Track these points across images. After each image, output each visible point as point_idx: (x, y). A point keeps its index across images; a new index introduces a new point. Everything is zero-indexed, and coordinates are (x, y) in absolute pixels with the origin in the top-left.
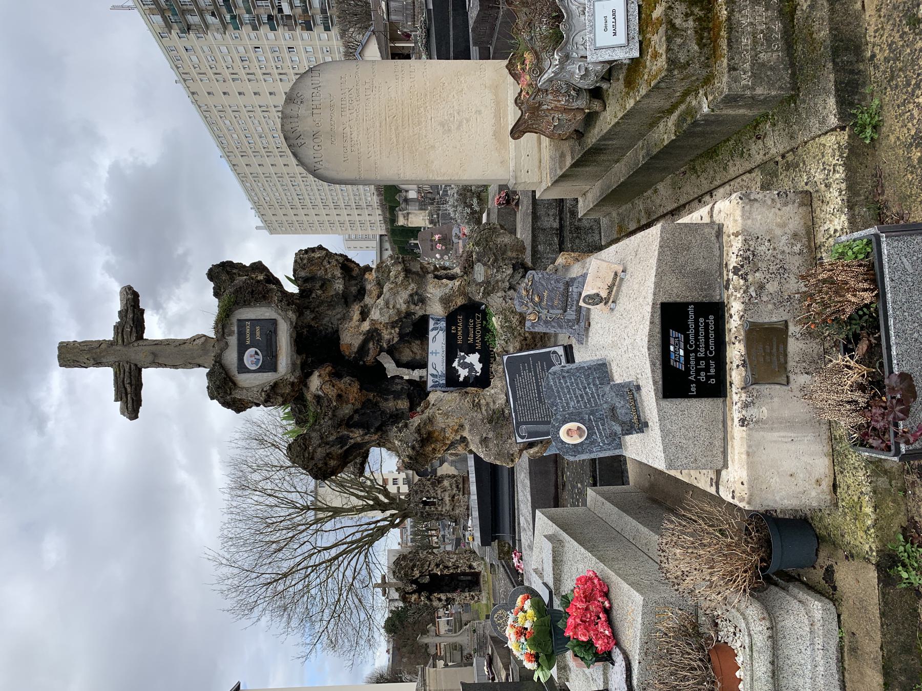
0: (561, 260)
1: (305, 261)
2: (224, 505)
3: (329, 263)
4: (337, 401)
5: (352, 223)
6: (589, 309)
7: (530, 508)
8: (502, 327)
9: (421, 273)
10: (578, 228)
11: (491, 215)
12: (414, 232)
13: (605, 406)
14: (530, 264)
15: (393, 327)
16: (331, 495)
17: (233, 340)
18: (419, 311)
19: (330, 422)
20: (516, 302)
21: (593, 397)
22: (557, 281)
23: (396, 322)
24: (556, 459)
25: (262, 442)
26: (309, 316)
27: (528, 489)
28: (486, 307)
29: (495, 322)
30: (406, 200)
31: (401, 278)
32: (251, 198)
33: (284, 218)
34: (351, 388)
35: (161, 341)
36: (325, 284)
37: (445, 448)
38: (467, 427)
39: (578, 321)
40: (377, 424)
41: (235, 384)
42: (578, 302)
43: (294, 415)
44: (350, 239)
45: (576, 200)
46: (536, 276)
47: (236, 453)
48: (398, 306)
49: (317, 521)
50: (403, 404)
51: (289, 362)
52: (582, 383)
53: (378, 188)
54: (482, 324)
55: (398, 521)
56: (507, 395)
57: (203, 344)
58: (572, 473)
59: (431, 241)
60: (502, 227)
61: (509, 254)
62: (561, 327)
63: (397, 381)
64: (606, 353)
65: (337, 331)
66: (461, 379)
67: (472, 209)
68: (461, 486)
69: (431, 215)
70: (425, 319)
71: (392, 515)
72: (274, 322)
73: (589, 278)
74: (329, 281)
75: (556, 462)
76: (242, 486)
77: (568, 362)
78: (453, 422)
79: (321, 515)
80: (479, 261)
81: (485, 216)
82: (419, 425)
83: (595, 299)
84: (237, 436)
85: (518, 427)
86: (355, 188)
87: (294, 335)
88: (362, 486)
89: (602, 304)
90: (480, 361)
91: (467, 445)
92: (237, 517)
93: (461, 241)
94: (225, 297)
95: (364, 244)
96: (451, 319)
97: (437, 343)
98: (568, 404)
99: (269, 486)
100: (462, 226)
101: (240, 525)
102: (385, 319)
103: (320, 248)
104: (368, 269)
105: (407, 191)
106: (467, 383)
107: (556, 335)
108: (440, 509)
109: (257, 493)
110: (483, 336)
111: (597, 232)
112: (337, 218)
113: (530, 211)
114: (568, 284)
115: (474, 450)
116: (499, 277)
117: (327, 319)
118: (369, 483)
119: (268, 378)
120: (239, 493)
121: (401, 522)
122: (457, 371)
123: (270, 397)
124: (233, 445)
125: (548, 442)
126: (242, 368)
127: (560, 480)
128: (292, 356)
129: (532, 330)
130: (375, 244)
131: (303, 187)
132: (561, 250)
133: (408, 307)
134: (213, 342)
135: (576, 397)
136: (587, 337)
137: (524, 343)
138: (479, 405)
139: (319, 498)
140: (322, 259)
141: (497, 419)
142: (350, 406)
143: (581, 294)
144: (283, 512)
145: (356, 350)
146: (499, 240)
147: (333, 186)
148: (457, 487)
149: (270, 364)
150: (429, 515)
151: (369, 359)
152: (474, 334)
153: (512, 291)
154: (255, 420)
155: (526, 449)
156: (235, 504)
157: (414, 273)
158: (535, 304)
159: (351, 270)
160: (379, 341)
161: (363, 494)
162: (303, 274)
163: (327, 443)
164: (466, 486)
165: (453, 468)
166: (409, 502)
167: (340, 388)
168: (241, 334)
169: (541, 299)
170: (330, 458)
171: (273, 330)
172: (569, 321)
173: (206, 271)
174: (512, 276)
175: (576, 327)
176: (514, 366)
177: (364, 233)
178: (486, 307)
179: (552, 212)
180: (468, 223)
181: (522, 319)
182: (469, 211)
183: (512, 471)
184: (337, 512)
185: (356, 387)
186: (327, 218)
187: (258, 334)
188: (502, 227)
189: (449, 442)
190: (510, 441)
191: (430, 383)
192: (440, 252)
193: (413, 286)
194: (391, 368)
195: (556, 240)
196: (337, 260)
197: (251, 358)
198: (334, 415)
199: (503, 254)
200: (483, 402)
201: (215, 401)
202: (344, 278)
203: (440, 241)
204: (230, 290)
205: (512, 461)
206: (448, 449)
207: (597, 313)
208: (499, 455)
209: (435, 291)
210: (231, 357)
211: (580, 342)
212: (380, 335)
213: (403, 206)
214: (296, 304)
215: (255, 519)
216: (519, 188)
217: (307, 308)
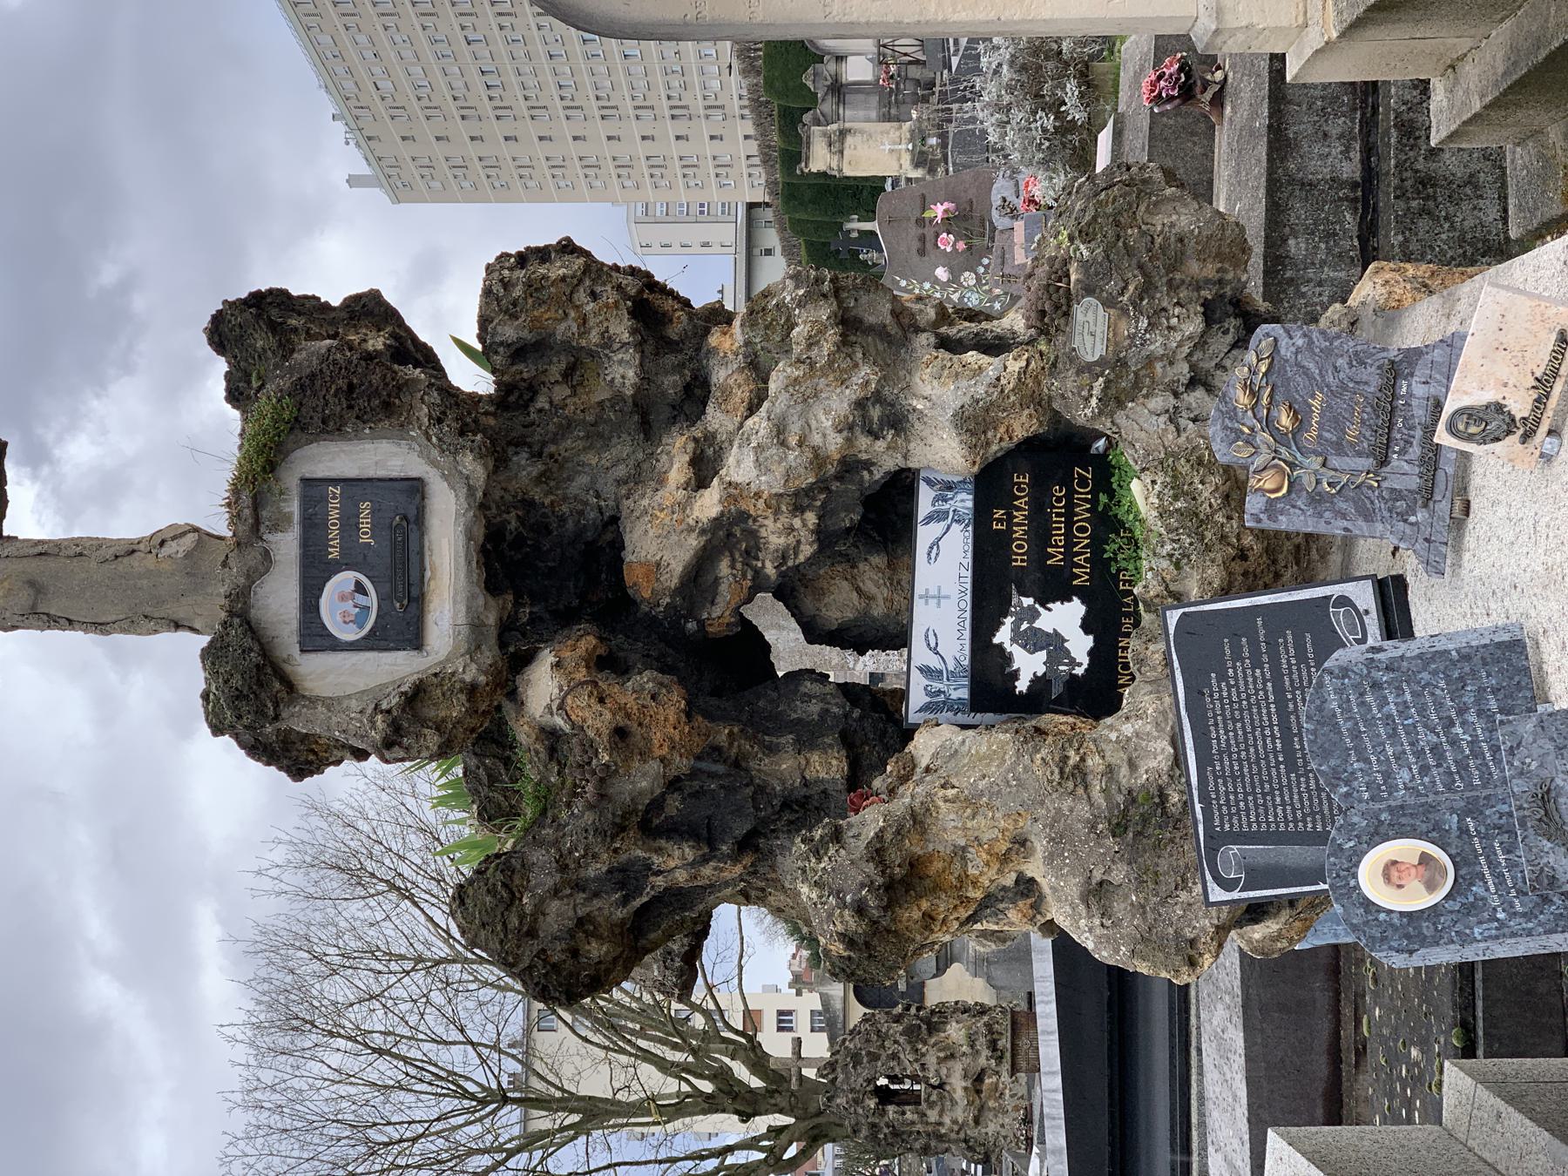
0: (1369, 289)
1: (518, 292)
2: (234, 1080)
3: (594, 296)
4: (613, 748)
5: (657, 165)
6: (1466, 456)
7: (1244, 1126)
8: (1163, 514)
9: (893, 329)
10: (1425, 182)
11: (1128, 135)
12: (863, 194)
13: (1518, 786)
14: (1263, 306)
15: (798, 509)
16: (577, 1058)
17: (286, 545)
18: (884, 457)
19: (589, 817)
20: (1214, 430)
21: (1477, 754)
22: (1359, 360)
23: (809, 492)
24: (1336, 963)
25: (357, 877)
26: (525, 469)
27: (1239, 1062)
28: (1111, 444)
29: (1142, 496)
30: (838, 89)
31: (827, 347)
32: (332, 84)
33: (439, 150)
34: (657, 704)
35: (58, 544)
36: (580, 365)
37: (964, 914)
38: (1040, 845)
39: (1427, 495)
40: (748, 833)
41: (290, 686)
42: (1430, 431)
43: (475, 792)
44: (647, 216)
45: (1423, 87)
46: (1284, 342)
47: (270, 909)
48: (816, 439)
49: (530, 1141)
50: (827, 766)
51: (462, 619)
52: (1439, 705)
53: (745, 51)
54: (1094, 501)
55: (791, 1152)
56: (1176, 741)
57: (188, 555)
58: (1389, 1010)
59: (921, 222)
60: (1170, 176)
61: (1193, 267)
62: (1368, 516)
63: (808, 686)
64: (1525, 604)
65: (615, 520)
66: (1022, 685)
67: (1059, 116)
68: (1004, 1043)
69: (919, 136)
70: (902, 485)
71: (775, 1132)
72: (415, 488)
73: (1470, 353)
74: (592, 354)
75: (1335, 971)
76: (291, 1018)
77: (1389, 634)
78: (991, 827)
79: (542, 1121)
80: (1089, 291)
81: (1105, 139)
82: (879, 836)
83: (1490, 422)
84: (279, 855)
85: (1212, 851)
86: (669, 47)
87: (480, 532)
88: (676, 1030)
89: (1514, 439)
90: (1086, 626)
91: (1037, 907)
92: (276, 1121)
93: (1019, 226)
94: (264, 404)
95: (695, 233)
96: (990, 484)
97: (943, 562)
98: (1388, 775)
99: (377, 1021)
100: (1025, 173)
101: (284, 1147)
102: (771, 483)
103: (567, 247)
104: (717, 316)
105: (840, 58)
106: (1039, 699)
107: (1348, 543)
108: (933, 1116)
109: (341, 1043)
110: (1097, 544)
111: (1490, 193)
112: (609, 149)
113: (1262, 122)
114: (1395, 371)
115: (1063, 922)
116: (1156, 345)
117: (583, 480)
118: (699, 1022)
119: (396, 668)
120: (284, 1041)
121: (804, 1155)
122: (1009, 659)
123: (403, 727)
124: (266, 883)
125: (1318, 903)
126: (315, 637)
127: (1347, 1032)
128: (471, 598)
129: (1267, 524)
130: (729, 233)
131: (501, 48)
132: (1368, 255)
133: (849, 441)
134: (220, 551)
135: (1419, 754)
136: (1458, 550)
137: (1237, 567)
138: (1080, 774)
139: (538, 1066)
140: (570, 284)
141: (1143, 821)
142: (654, 767)
143: (1438, 406)
144: (424, 1108)
145: (674, 583)
146: (1159, 221)
147: (599, 44)
148: (993, 1045)
149: (401, 625)
150: (896, 1134)
151: (718, 614)
152: (1068, 535)
153: (1199, 393)
154: (336, 806)
155: (1239, 924)
156: (268, 1077)
157: (871, 330)
158: (1280, 437)
159: (663, 319)
160: (752, 552)
161: (679, 1057)
162: (509, 332)
163: (579, 886)
164: (1024, 1043)
165: (980, 982)
166: (831, 1090)
167: (622, 708)
168: (312, 527)
169: (1300, 418)
170: (588, 934)
171: (412, 513)
172: (1397, 495)
173: (206, 321)
174: (1201, 343)
175: (1420, 516)
176: (1202, 645)
177: (698, 197)
178: (1111, 444)
179: (1336, 126)
180: (1044, 163)
181: (1235, 487)
182: (1050, 122)
183: (1181, 998)
184: (596, 1113)
185: (675, 701)
186: (575, 150)
187: (365, 526)
188: (1170, 176)
189: (978, 894)
190: (1184, 896)
191: (917, 698)
192: (950, 261)
193: (866, 373)
194: (788, 646)
195: (1350, 220)
196: (619, 288)
197: (344, 602)
198: (602, 796)
199: (1171, 268)
200: (1094, 762)
201: (227, 739)
202: (640, 346)
203: (949, 223)
204: (279, 382)
205: (1192, 963)
206: (973, 919)
207: (1495, 469)
208: (1146, 942)
209: (940, 391)
210: (279, 600)
211: (1435, 568)
212: (753, 535)
213: (827, 106)
214: (500, 427)
215: (333, 1130)
216: (1228, 48)
217: (519, 443)
